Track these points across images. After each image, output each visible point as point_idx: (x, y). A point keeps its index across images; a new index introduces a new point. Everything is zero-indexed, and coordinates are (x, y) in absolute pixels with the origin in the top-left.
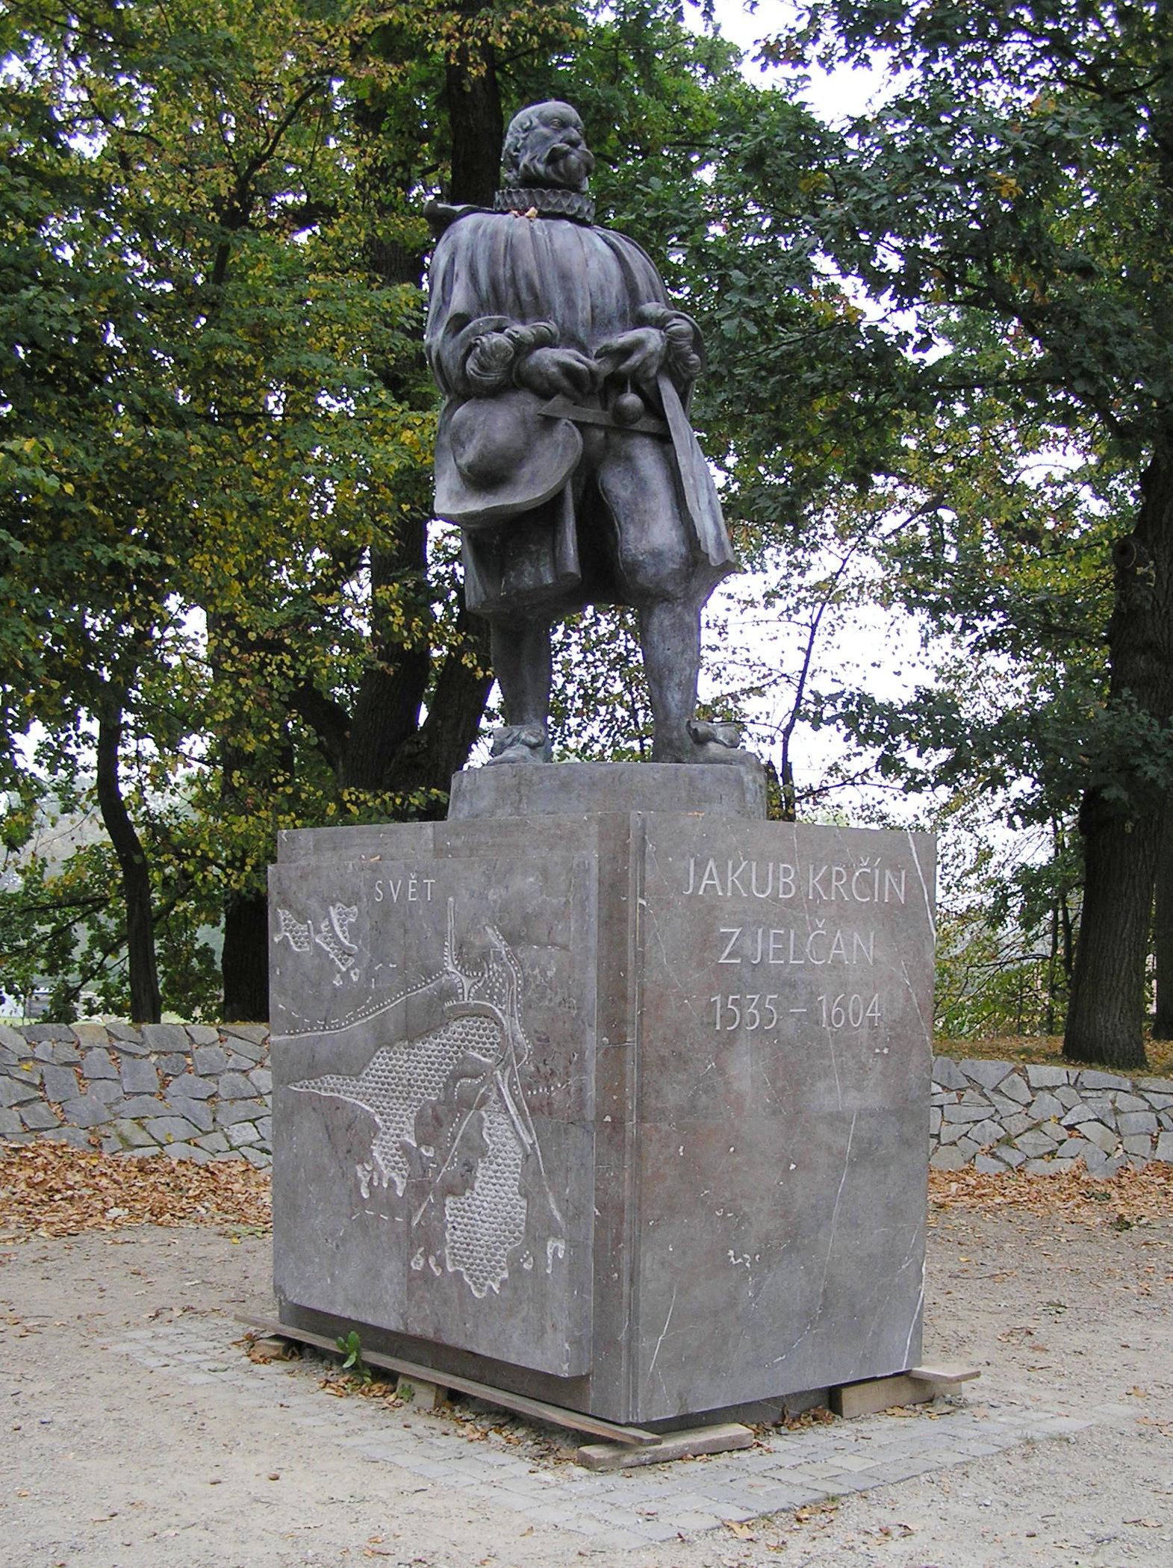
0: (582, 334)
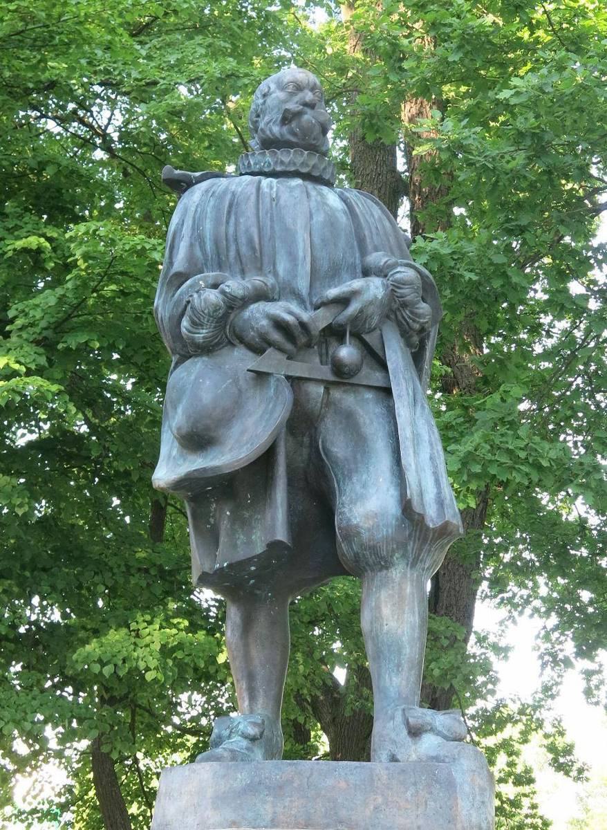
0: (303, 285)
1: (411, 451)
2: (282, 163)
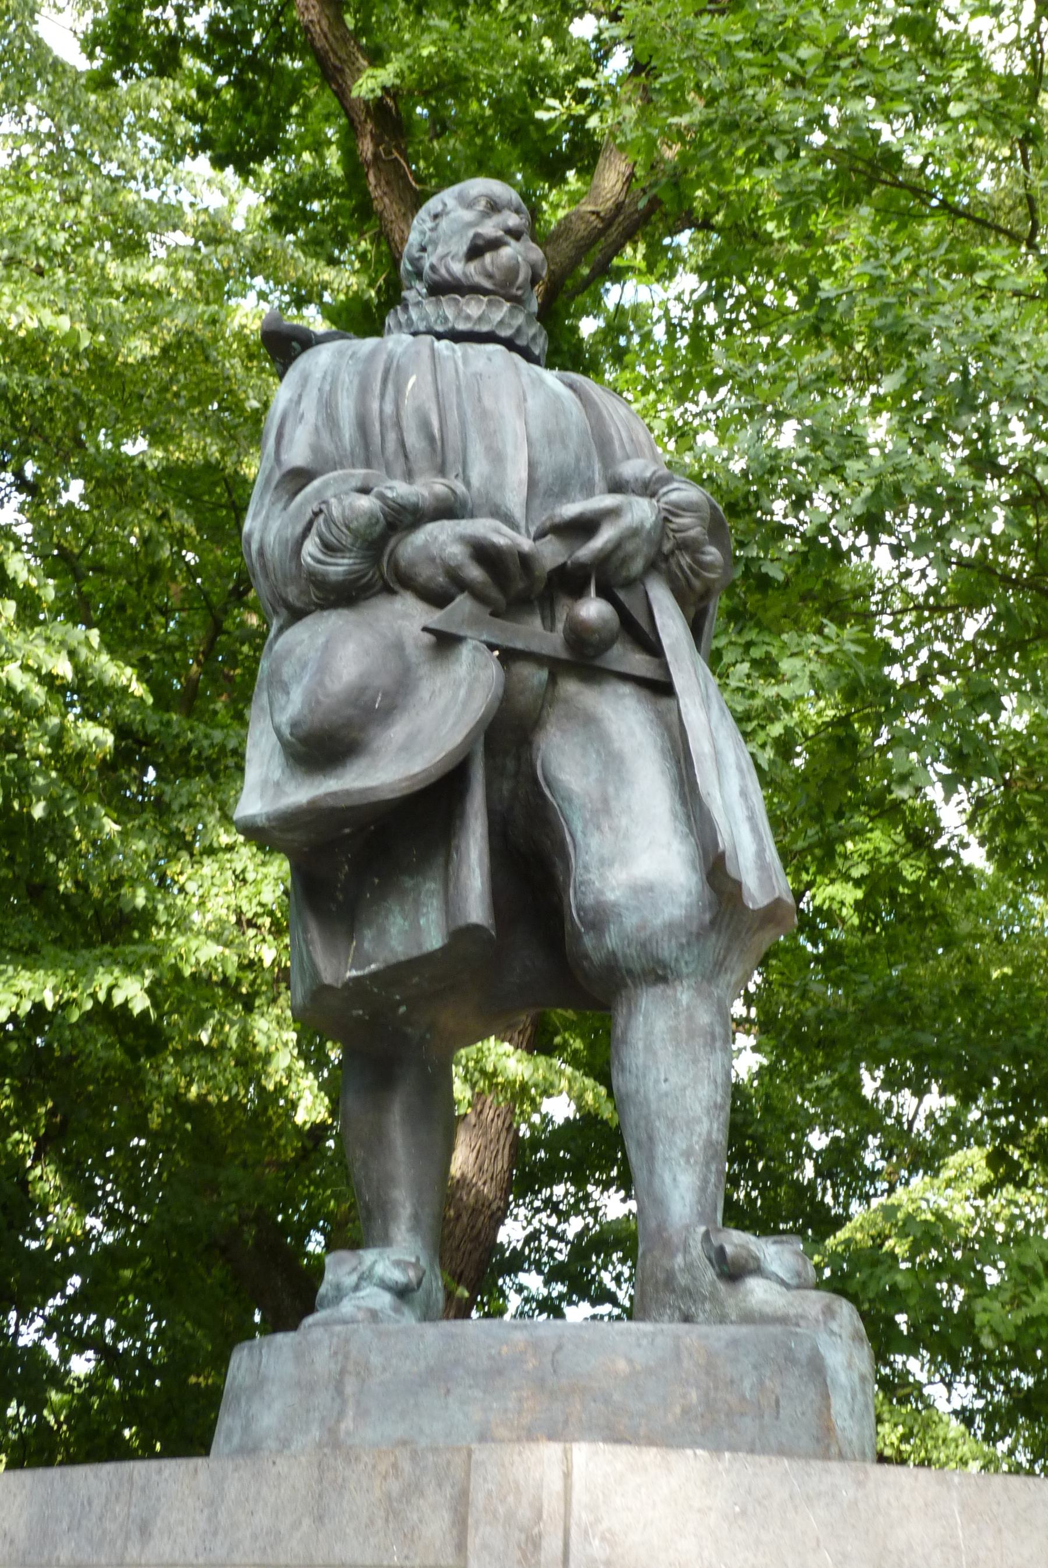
0: (515, 500)
1: (713, 777)
2: (468, 318)
